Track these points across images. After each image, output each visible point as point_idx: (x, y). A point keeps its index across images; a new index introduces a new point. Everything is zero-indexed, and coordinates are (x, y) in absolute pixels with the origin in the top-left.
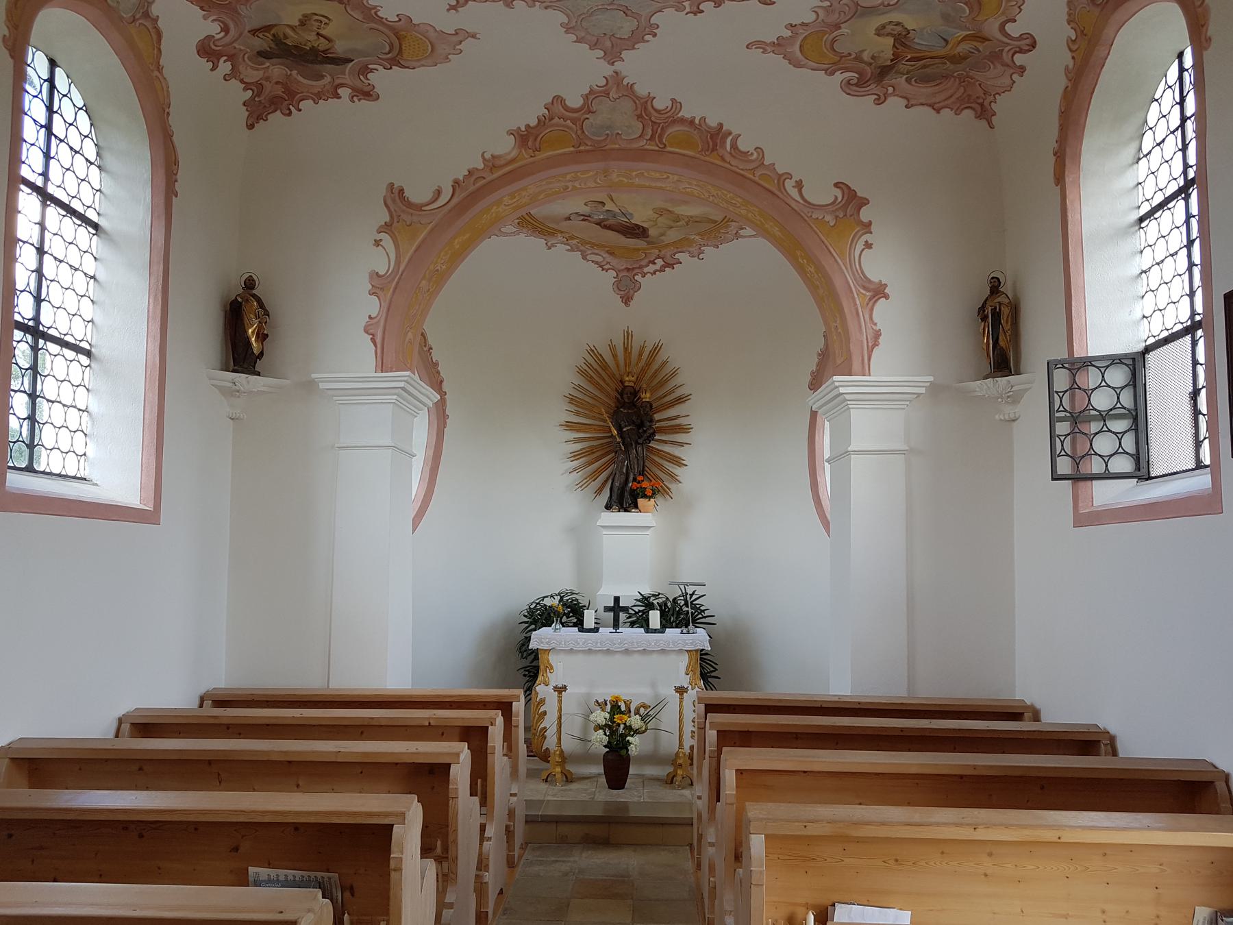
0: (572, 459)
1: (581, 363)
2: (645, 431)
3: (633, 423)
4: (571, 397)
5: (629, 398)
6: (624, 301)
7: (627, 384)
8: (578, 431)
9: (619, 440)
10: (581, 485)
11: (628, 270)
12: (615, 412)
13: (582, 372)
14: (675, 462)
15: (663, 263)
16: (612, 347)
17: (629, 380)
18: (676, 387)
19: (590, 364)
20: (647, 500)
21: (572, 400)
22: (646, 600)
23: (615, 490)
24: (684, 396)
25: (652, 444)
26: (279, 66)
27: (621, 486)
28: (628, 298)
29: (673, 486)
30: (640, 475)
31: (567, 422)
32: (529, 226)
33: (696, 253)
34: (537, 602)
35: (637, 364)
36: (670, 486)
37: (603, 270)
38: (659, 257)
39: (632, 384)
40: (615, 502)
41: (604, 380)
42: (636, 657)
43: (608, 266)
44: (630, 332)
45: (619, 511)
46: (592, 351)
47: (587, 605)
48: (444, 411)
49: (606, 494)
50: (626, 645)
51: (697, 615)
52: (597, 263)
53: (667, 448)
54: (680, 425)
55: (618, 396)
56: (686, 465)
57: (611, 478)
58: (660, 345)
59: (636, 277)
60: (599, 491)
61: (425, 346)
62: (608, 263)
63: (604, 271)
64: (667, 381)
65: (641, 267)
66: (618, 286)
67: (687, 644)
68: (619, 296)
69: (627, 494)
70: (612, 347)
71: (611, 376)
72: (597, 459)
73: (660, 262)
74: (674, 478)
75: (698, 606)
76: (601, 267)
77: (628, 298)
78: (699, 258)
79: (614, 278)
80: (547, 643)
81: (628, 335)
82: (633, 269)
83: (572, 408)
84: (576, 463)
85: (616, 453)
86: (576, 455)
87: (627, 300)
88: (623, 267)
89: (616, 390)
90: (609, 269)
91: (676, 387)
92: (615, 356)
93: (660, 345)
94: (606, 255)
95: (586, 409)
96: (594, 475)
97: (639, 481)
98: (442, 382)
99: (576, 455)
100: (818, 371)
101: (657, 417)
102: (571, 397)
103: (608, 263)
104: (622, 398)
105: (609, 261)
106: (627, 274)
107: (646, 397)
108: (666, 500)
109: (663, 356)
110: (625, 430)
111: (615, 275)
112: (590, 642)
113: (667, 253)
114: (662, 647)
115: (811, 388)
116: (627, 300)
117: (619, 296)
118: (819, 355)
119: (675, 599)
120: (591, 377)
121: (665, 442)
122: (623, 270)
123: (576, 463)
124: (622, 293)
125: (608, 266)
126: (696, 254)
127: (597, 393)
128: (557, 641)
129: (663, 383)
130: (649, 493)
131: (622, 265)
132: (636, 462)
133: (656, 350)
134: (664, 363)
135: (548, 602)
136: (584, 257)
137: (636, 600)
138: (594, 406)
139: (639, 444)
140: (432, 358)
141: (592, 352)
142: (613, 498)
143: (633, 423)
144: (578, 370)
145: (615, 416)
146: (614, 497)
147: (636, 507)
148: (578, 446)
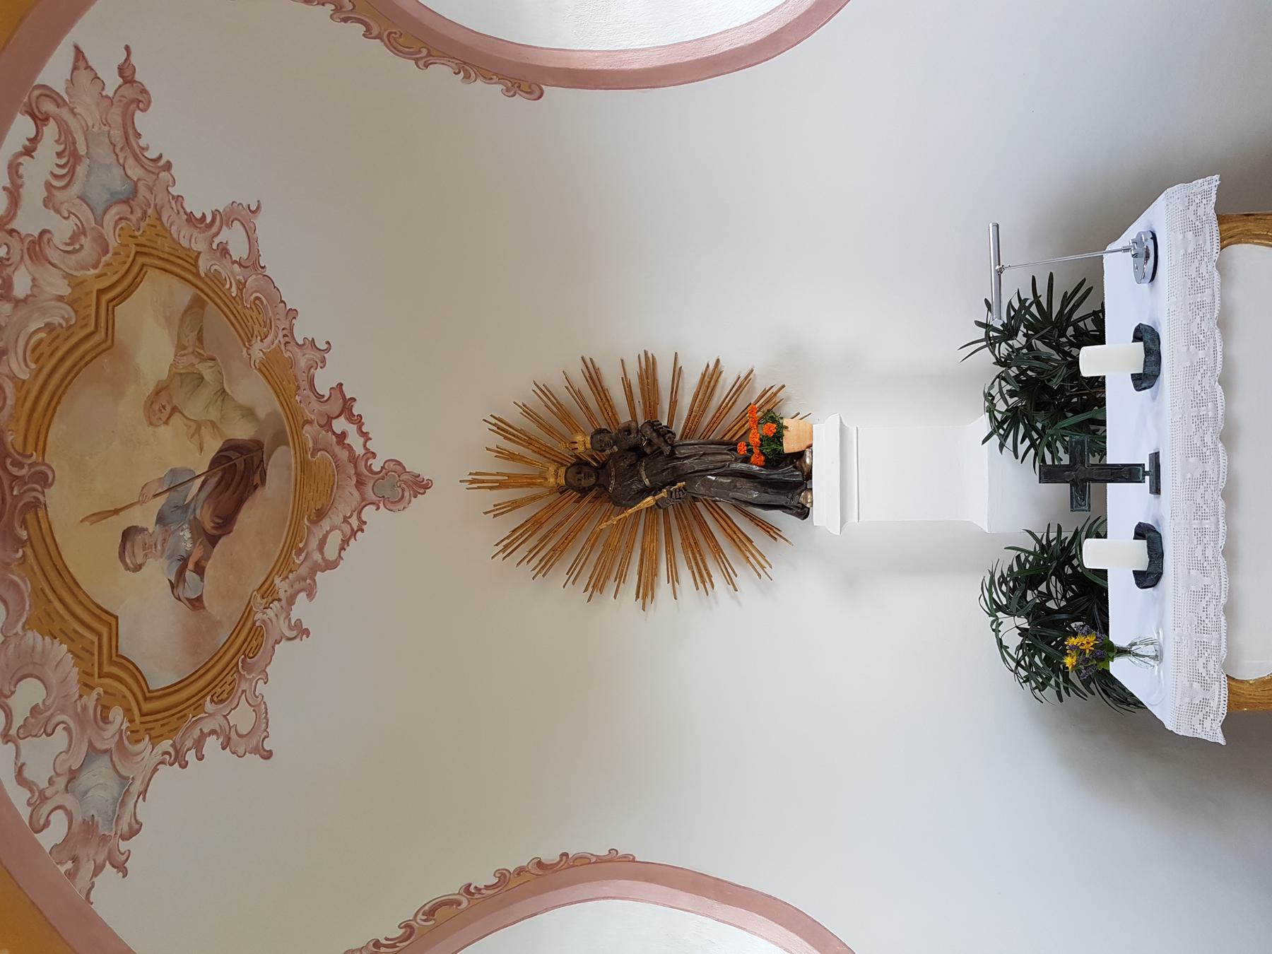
0: (708, 585)
1: (527, 569)
2: (650, 442)
3: (633, 466)
4: (590, 589)
5: (587, 476)
6: (422, 491)
7: (563, 482)
8: (655, 574)
9: (664, 494)
10: (760, 566)
11: (360, 484)
12: (616, 504)
13: (545, 567)
14: (712, 383)
15: (342, 418)
16: (499, 510)
17: (554, 476)
18: (570, 387)
19: (530, 551)
20: (785, 432)
21: (597, 585)
22: (1000, 425)
23: (767, 498)
24: (585, 370)
25: (678, 428)
26: (1217, 306)
27: (759, 486)
28: (416, 483)
29: (760, 385)
30: (735, 450)
31: (637, 597)
32: (229, 679)
33: (311, 354)
34: (1013, 665)
35: (530, 463)
36: (759, 393)
37: (362, 531)
38: (328, 426)
39: (562, 471)
40: (792, 499)
41: (560, 524)
42: (1244, 408)
43: (354, 522)
44: (470, 478)
45: (811, 489)
46: (506, 547)
47: (1016, 553)
48: (600, 860)
49: (776, 517)
50: (1208, 439)
51: (1032, 315)
52: (345, 542)
53: (686, 401)
54: (640, 377)
55: (588, 498)
56: (718, 361)
57: (743, 506)
58: (494, 421)
59: (376, 468)
60: (771, 531)
61: (459, 903)
62: (346, 520)
63: (364, 527)
64: (559, 405)
65: (354, 460)
66: (394, 502)
67: (1199, 248)
68: (413, 499)
69: (776, 475)
70: (499, 510)
71: (551, 509)
72: (709, 535)
73: (340, 425)
74: (742, 385)
75: (1012, 313)
76: (354, 533)
77: (416, 483)
78: (328, 350)
79: (378, 508)
80: (1206, 686)
81: (477, 481)
82: (358, 474)
83: (611, 585)
84: (718, 578)
85: (695, 499)
86: (702, 578)
87: (420, 485)
88: (356, 493)
89: (578, 501)
90: (359, 518)
91: (570, 387)
92: (514, 505)
93: (494, 421)
94: (326, 524)
95: (614, 558)
96: (741, 542)
97: (748, 450)
98: (540, 864)
99: (702, 578)
100: (502, 78)
101: (624, 417)
102: (590, 589)
103: (346, 520)
104: (590, 489)
105: (341, 517)
106: (371, 485)
107: (582, 442)
108: (788, 398)
109: (515, 417)
110: (647, 482)
111: (373, 507)
112: (1198, 553)
113: (312, 409)
114: (1209, 325)
115: (537, 93)
116: (420, 485)
117: (413, 499)
118: (467, 76)
119: (999, 362)
120: (554, 550)
121: (674, 403)
122: (362, 494)
123: (718, 578)
124: (407, 494)
125: (354, 522)
126: (318, 354)
127: (583, 538)
128: (1200, 655)
129: (563, 413)
130: (769, 429)
131: (350, 495)
132: (710, 458)
133: (501, 427)
134: (527, 411)
135: (1013, 640)
136: (332, 565)
137: (1001, 450)
138: (607, 545)
139: (672, 452)
140: (487, 887)
141: (507, 548)
142: (783, 503)
143: (633, 466)
144: (540, 575)
145: (621, 501)
146: (782, 500)
147: (800, 455)
148: (685, 574)
